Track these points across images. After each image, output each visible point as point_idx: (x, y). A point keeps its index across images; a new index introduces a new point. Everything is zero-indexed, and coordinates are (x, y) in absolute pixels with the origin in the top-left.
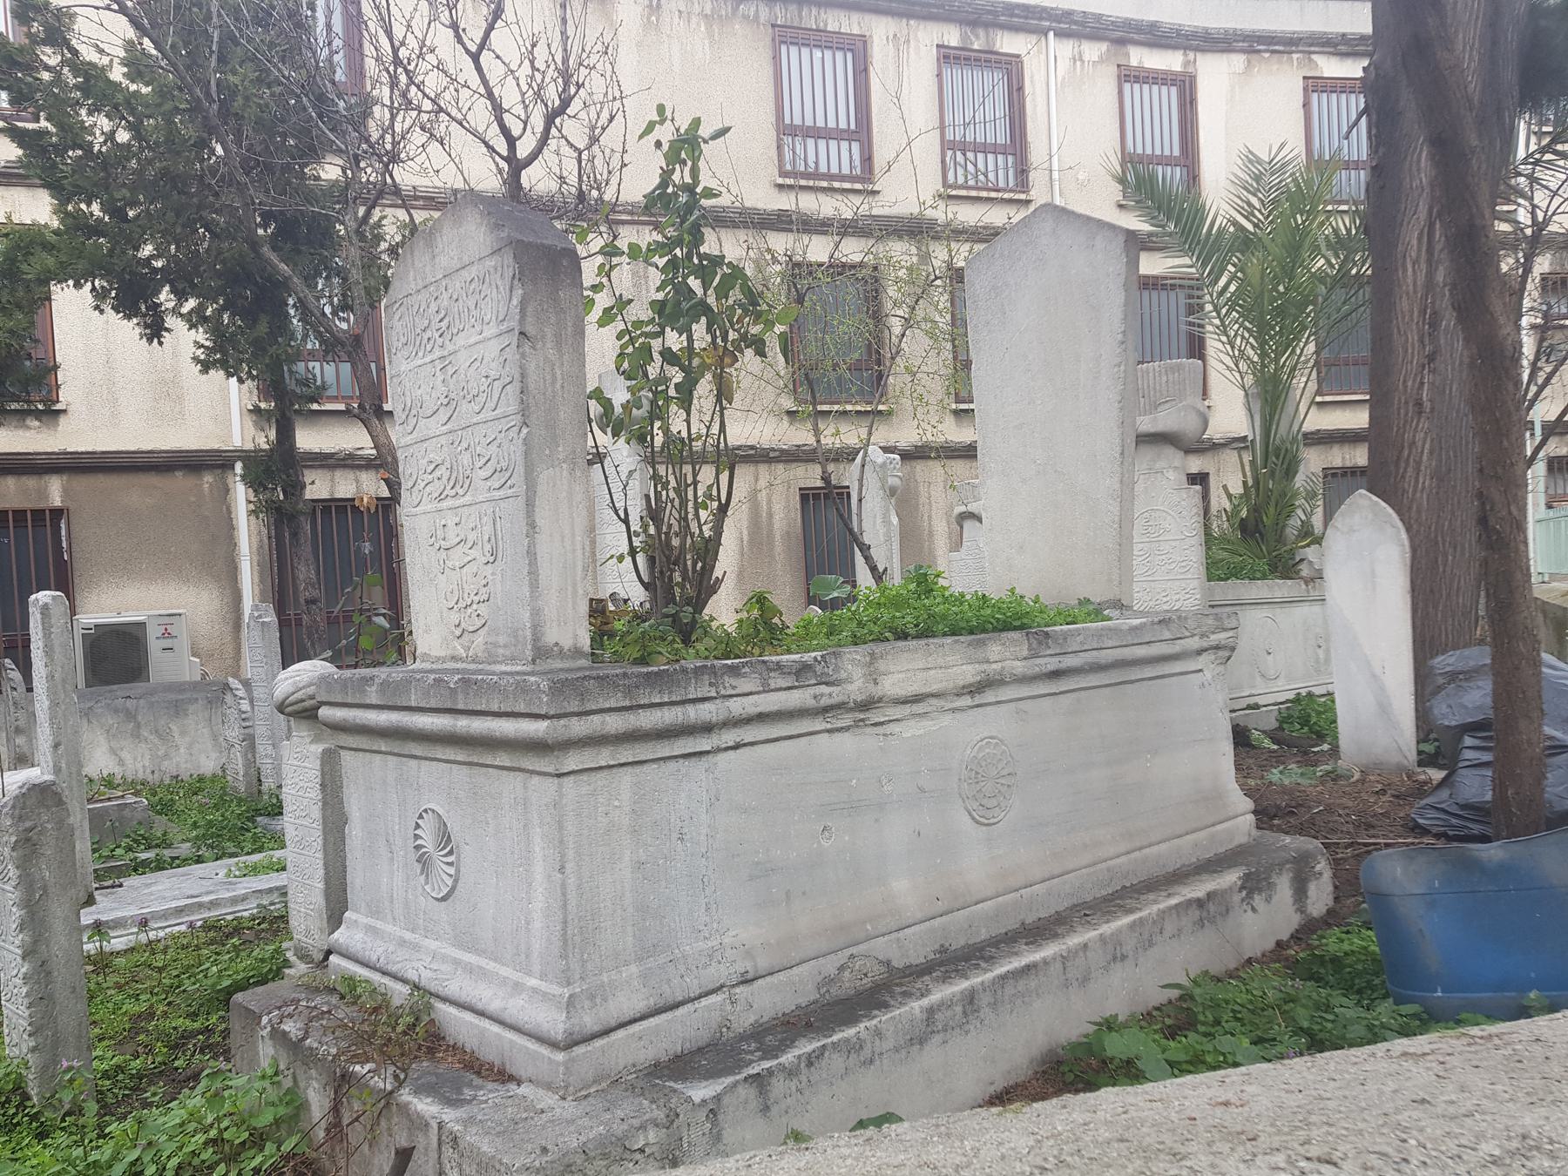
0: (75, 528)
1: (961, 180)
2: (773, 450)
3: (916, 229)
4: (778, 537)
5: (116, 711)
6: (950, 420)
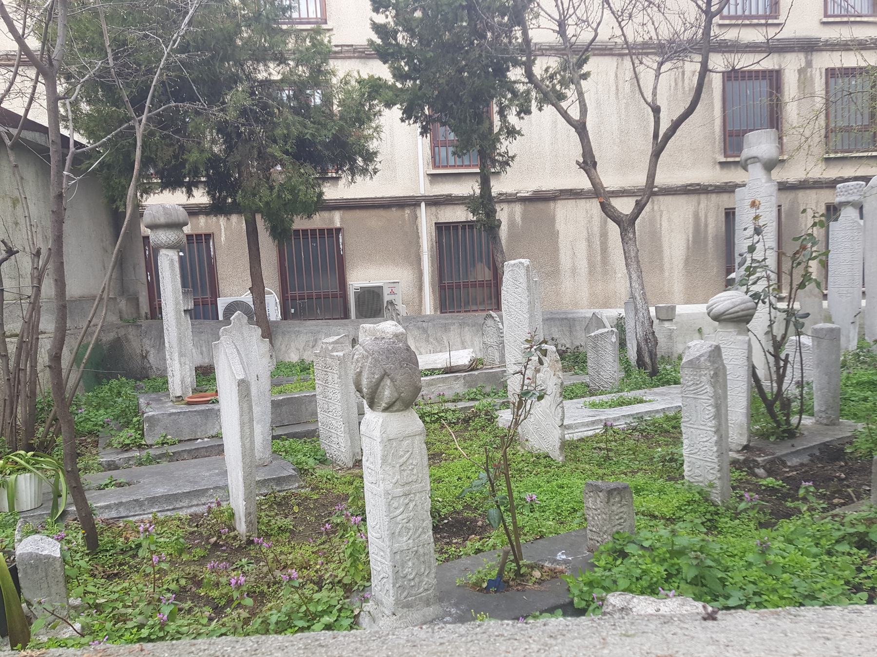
0: (347, 238)
1: (740, 13)
2: (711, 186)
3: (809, 47)
4: (710, 238)
5: (419, 328)
6: (822, 165)
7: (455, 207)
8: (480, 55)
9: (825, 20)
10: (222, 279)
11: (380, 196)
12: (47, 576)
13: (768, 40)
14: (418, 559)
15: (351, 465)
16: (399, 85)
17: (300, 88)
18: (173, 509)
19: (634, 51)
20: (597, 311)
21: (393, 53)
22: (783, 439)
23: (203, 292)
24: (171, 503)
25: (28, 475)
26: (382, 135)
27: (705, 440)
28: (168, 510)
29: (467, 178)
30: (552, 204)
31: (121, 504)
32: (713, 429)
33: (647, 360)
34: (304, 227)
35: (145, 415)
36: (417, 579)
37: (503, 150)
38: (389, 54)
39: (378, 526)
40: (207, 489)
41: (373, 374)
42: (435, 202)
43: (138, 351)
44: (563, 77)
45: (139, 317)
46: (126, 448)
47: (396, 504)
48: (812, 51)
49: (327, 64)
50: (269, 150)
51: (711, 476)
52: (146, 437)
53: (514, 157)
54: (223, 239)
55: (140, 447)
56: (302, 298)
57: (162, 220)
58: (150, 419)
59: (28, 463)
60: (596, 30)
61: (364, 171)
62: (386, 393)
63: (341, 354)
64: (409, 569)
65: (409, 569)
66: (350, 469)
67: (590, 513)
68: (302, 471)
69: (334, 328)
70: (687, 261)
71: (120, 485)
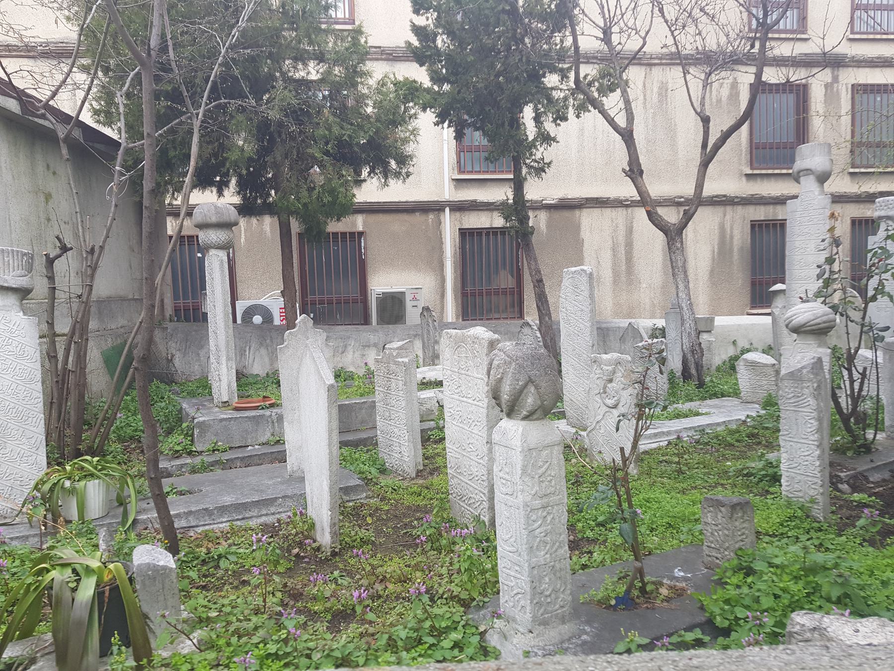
0: (369, 243)
2: (737, 197)
3: (833, 62)
4: (735, 250)
6: (847, 178)
7: (480, 213)
8: (520, 60)
9: (852, 36)
10: (241, 282)
11: (404, 200)
12: (163, 588)
13: (824, 54)
14: (555, 574)
15: (414, 475)
16: (436, 88)
17: (336, 89)
18: (243, 519)
19: (678, 59)
20: (633, 321)
21: (430, 56)
22: (859, 454)
23: (185, 297)
24: (240, 513)
25: (97, 481)
26: (418, 138)
27: (806, 453)
28: (238, 520)
29: (493, 184)
30: (577, 212)
31: (190, 512)
32: (816, 443)
33: (693, 371)
34: (335, 230)
35: (196, 421)
36: (553, 596)
37: (538, 156)
38: (426, 57)
39: (513, 539)
40: (276, 498)
41: (518, 380)
42: (459, 207)
43: (164, 355)
44: (601, 85)
45: (164, 319)
46: (177, 455)
47: (534, 517)
48: (838, 67)
49: (364, 65)
50: (309, 150)
51: (813, 491)
52: (196, 444)
53: (550, 163)
54: (243, 240)
55: (190, 453)
56: (321, 302)
57: (214, 219)
58: (201, 425)
59: (96, 468)
60: (644, 39)
61: (397, 175)
62: (529, 401)
63: (406, 360)
64: (545, 586)
65: (545, 586)
66: (413, 479)
67: (708, 528)
68: (368, 481)
69: (364, 334)
70: (712, 273)
71: (181, 493)
